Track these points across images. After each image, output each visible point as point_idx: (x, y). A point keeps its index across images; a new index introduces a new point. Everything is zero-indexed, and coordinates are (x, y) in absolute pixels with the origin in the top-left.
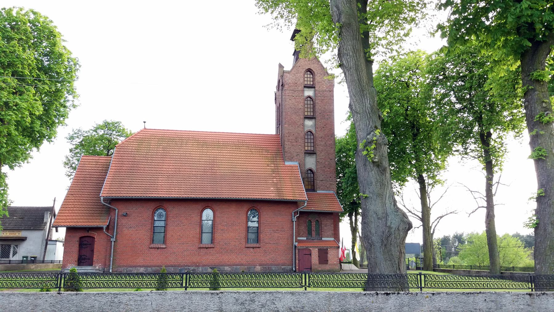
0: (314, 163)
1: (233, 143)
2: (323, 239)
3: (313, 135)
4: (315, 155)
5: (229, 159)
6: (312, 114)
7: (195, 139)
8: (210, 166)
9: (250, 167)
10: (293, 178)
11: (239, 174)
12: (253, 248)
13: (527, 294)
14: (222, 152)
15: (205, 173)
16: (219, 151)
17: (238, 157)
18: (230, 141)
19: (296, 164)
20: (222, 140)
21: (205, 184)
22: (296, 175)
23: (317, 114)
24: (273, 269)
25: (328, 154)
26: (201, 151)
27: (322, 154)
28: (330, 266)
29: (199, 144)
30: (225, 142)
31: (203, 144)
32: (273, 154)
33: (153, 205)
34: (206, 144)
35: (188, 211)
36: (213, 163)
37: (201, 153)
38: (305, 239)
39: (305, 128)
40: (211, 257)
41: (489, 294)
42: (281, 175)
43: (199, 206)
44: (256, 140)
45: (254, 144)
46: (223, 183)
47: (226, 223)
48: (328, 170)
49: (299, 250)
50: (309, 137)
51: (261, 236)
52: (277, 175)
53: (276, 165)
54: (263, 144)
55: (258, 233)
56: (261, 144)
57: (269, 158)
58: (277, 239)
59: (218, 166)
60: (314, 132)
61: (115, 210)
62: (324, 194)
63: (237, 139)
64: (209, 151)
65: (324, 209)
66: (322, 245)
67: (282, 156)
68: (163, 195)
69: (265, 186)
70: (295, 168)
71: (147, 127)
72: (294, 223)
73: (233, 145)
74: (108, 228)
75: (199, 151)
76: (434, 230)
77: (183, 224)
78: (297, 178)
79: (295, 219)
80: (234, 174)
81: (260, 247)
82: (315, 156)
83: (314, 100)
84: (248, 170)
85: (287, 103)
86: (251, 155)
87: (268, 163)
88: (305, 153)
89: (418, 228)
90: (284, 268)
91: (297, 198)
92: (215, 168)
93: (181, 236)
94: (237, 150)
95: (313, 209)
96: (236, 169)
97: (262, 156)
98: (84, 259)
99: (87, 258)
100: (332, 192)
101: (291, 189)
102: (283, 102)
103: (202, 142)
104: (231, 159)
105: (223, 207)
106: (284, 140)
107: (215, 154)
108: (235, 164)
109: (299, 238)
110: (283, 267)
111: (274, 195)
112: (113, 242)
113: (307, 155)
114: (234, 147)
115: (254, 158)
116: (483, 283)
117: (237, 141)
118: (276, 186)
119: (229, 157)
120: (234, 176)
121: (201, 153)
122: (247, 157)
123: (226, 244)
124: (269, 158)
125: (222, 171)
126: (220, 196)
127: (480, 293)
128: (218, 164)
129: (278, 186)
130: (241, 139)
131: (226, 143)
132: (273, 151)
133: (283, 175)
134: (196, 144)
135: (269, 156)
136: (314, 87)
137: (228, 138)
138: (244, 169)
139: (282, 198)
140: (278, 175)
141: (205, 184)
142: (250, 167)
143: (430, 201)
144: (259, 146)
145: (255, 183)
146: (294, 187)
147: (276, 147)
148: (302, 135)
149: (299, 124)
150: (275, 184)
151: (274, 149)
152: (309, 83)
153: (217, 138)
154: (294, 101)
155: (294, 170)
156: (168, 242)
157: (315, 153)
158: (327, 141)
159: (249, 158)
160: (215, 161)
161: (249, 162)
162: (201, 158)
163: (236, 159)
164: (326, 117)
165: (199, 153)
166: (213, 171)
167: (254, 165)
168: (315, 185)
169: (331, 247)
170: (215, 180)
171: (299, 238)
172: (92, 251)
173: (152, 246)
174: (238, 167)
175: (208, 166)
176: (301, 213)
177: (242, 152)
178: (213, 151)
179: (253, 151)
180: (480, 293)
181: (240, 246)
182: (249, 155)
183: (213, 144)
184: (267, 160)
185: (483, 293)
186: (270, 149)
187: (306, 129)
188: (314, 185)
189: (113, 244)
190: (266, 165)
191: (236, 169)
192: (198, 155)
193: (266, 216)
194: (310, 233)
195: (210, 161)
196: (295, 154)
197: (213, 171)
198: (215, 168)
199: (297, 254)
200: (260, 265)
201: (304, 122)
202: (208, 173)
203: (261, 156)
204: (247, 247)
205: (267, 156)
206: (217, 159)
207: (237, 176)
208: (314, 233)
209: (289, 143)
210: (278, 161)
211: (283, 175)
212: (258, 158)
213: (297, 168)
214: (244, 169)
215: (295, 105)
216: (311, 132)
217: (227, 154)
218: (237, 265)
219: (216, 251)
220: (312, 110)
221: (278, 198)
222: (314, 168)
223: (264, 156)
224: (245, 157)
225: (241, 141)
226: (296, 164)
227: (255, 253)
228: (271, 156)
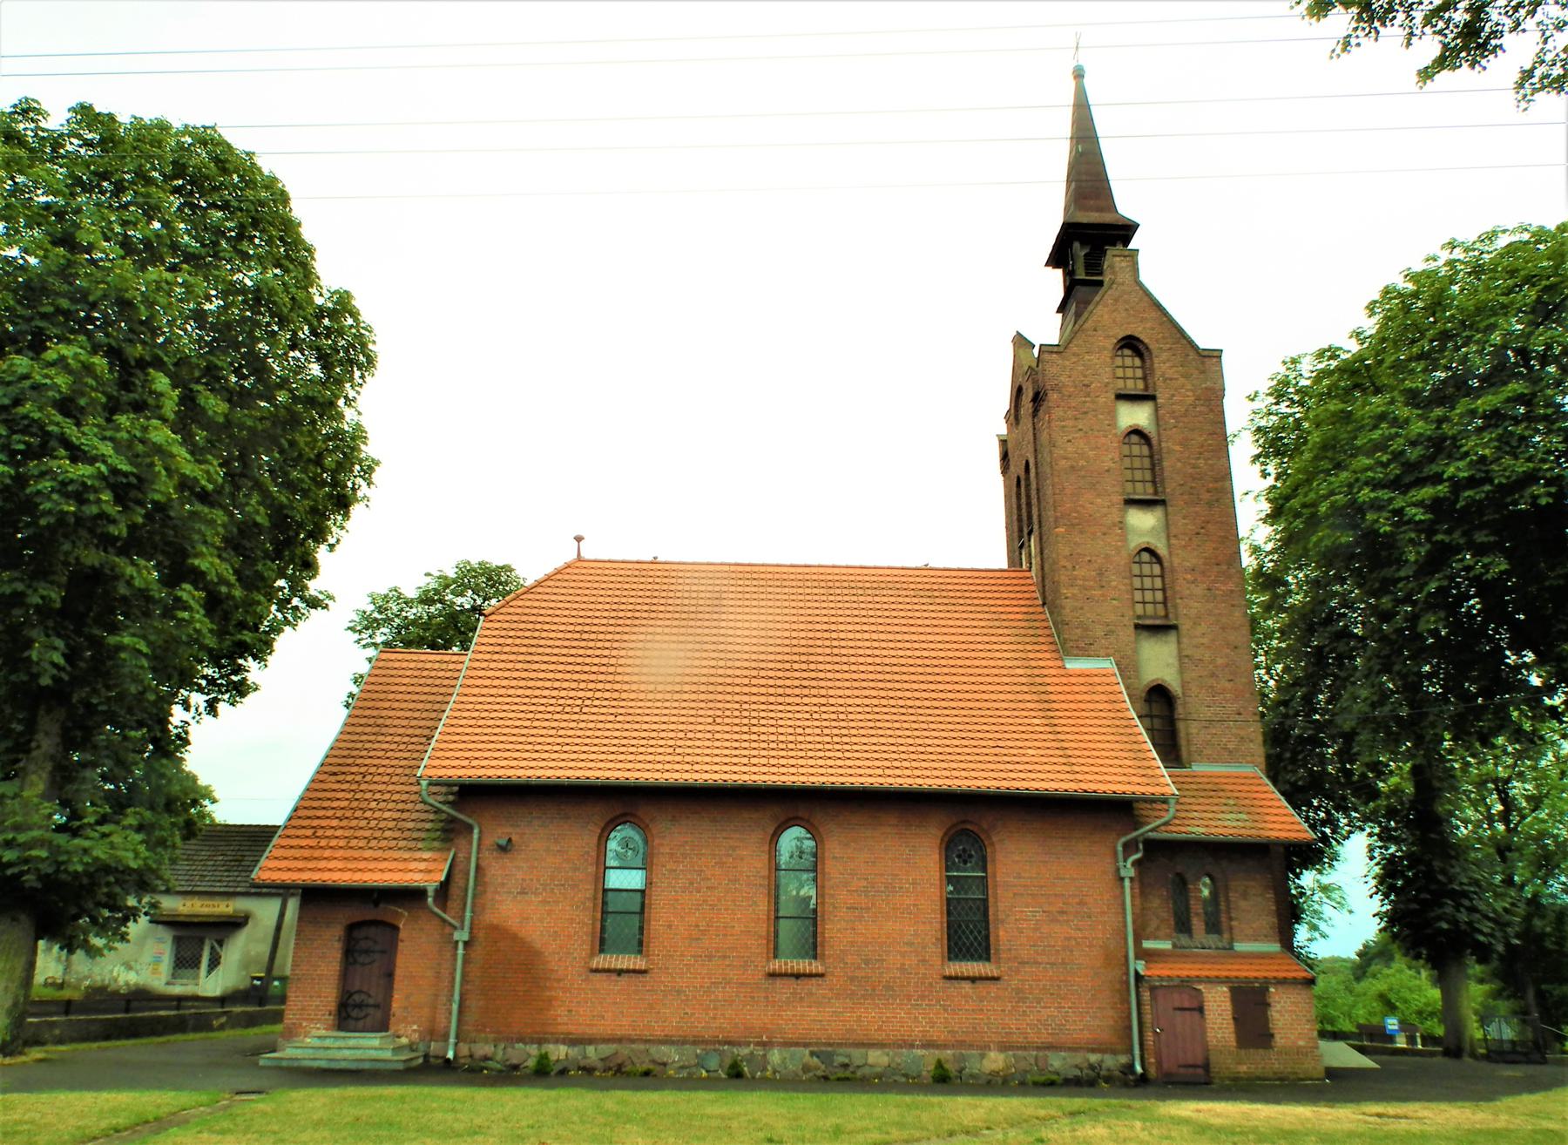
0: (1173, 661)
23: (1171, 487)
33: (598, 813)
35: (724, 834)
40: (813, 1013)
43: (768, 816)
48: (1228, 685)
49: (1153, 989)
51: (1001, 933)
60: (1162, 550)
61: (470, 828)
67: (1049, 639)
68: (608, 774)
71: (586, 555)
72: (1127, 883)
74: (444, 889)
77: (709, 884)
79: (1129, 871)
83: (1154, 442)
85: (1058, 452)
93: (703, 924)
98: (360, 1006)
99: (371, 1001)
102: (1045, 456)
106: (1056, 583)
109: (1147, 944)
112: (461, 945)
113: (1145, 634)
123: (867, 962)
147: (1024, 609)
152: (1130, 384)
156: (655, 947)
157: (1174, 627)
169: (1282, 982)
172: (390, 975)
173: (601, 961)
187: (1135, 542)
189: (460, 951)
194: (1183, 925)
199: (1147, 1008)
200: (1003, 1047)
201: (1123, 517)
208: (1198, 924)
209: (1075, 591)
222: (1171, 679)
226: (1108, 665)
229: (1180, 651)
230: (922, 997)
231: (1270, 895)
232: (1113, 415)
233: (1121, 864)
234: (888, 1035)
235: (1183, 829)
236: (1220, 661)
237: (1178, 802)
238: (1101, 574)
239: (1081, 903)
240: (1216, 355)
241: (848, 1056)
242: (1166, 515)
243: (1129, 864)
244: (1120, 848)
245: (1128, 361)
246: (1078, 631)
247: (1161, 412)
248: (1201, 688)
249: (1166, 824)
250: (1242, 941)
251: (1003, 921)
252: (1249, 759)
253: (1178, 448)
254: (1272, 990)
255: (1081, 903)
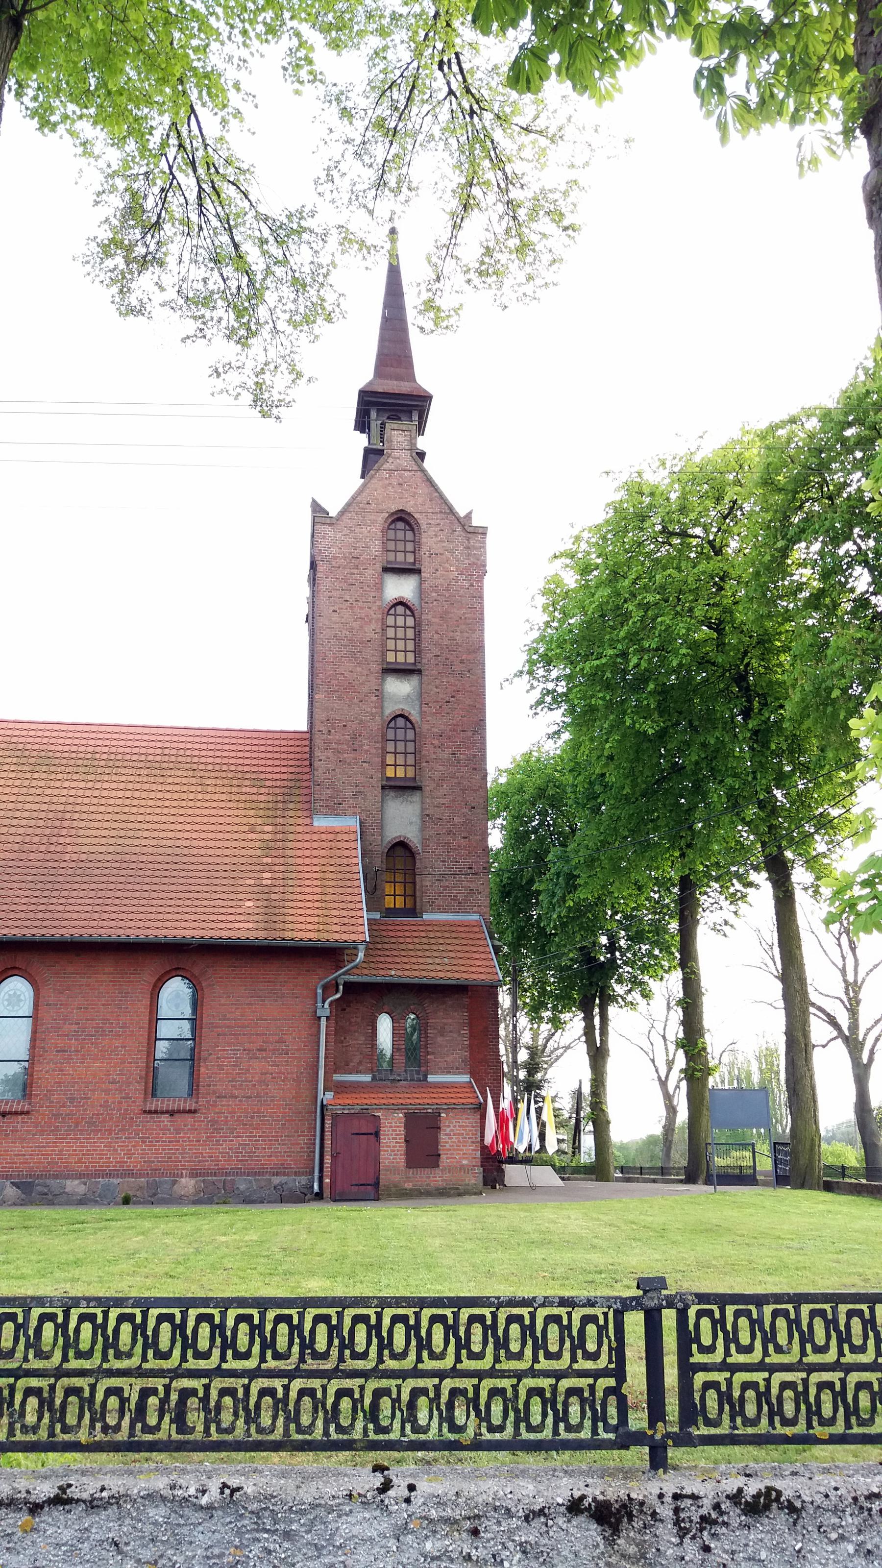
0: (416, 819)
1: (143, 758)
2: (431, 1078)
3: (414, 728)
4: (418, 793)
5: (117, 809)
6: (411, 658)
7: (12, 746)
8: (47, 831)
9: (186, 835)
10: (332, 869)
11: (144, 858)
12: (172, 1113)
13: (575, 1507)
14: (98, 785)
15: (23, 856)
16: (90, 785)
17: (151, 803)
18: (136, 750)
19: (353, 823)
20: (106, 749)
21: (10, 893)
22: (345, 861)
23: (427, 657)
24: (242, 1187)
25: (463, 790)
26: (26, 783)
27: (442, 792)
28: (447, 1176)
29: (23, 760)
30: (116, 754)
31: (40, 761)
32: (277, 791)
34: (48, 761)
36: (57, 823)
37: (24, 791)
38: (367, 1078)
39: (386, 704)
40: (17, 1148)
41: (158, 1513)
42: (291, 861)
44: (226, 747)
45: (218, 760)
46: (76, 886)
47: (75, 1027)
49: (335, 1117)
50: (400, 734)
51: (202, 1070)
52: (277, 861)
53: (279, 828)
54: (270, 769)
55: (192, 1060)
56: (240, 761)
57: (262, 805)
58: (260, 1082)
59: (73, 832)
60: (415, 716)
62: (451, 924)
63: (160, 745)
64: (52, 784)
65: (433, 974)
66: (421, 1100)
69: (225, 896)
70: (346, 837)
72: (323, 1022)
73: (142, 765)
75: (18, 782)
76: (872, 1052)
78: (348, 869)
79: (325, 1010)
80: (127, 858)
81: (195, 1112)
82: (416, 797)
84: (179, 843)
86: (200, 796)
87: (252, 821)
88: (383, 787)
89: (824, 1046)
90: (281, 1185)
91: (334, 935)
92: (62, 840)
94: (152, 779)
95: (394, 974)
96: (136, 842)
97: (237, 797)
100: (475, 917)
101: (317, 905)
103: (35, 754)
104: (126, 809)
105: (70, 969)
107: (72, 792)
108: (138, 826)
109: (337, 1077)
110: (276, 1180)
111: (250, 925)
113: (392, 794)
114: (142, 772)
115: (207, 804)
116: (139, 1384)
117: (159, 751)
118: (265, 896)
119: (119, 802)
120: (125, 865)
121: (24, 791)
122: (184, 804)
123: (72, 1099)
124: (262, 805)
125: (85, 849)
126: (53, 931)
127: (61, 1500)
128: (75, 824)
129: (274, 897)
130: (175, 745)
131: (119, 757)
132: (278, 783)
133: (299, 861)
134: (15, 760)
135: (262, 798)
136: (418, 572)
137: (130, 743)
138: (163, 842)
139: (276, 934)
140: (282, 861)
141: (10, 893)
142: (186, 835)
143: (856, 961)
144: (233, 768)
145: (192, 888)
146: (327, 898)
147: (292, 770)
148: (375, 725)
149: (365, 689)
150: (266, 889)
151: (285, 776)
152: (400, 557)
153: (92, 742)
154: (347, 615)
155: (340, 845)
157: (418, 788)
158: (459, 747)
159: (191, 804)
160: (68, 816)
161: (189, 819)
162: (19, 806)
163: (142, 810)
164: (458, 667)
165: (16, 790)
166: (52, 848)
167: (204, 828)
168: (418, 894)
169: (451, 1108)
170: (50, 879)
171: (337, 1077)
174: (146, 834)
175: (38, 831)
176: (350, 987)
177: (169, 788)
178: (66, 784)
179: (209, 782)
180: (61, 1500)
181: (124, 1106)
182: (192, 796)
183: (72, 762)
184: (252, 813)
185: (93, 1505)
186: (269, 776)
187: (390, 709)
188: (414, 896)
190: (246, 828)
191: (136, 842)
192: (13, 798)
193: (223, 1001)
195: (51, 815)
196: (349, 791)
197: (52, 848)
198: (62, 840)
199: (328, 1135)
200: (194, 1174)
201: (382, 684)
202: (32, 856)
203: (233, 797)
204: (150, 1112)
205: (254, 797)
206: (78, 808)
207: (133, 865)
209: (329, 753)
210: (291, 813)
211: (299, 861)
212: (222, 805)
213: (352, 837)
214: (163, 842)
215: (351, 630)
216: (407, 719)
217: (113, 794)
218: (110, 1175)
219: (36, 1125)
220: (411, 646)
221: (261, 934)
222: (412, 835)
223: (243, 797)
224: (175, 804)
225: (174, 752)
227: (178, 1131)
228: (270, 798)
229: (423, 809)
230: (123, 1130)
231: (465, 1031)
232: (380, 587)
233: (319, 1004)
234: (86, 1167)
235: (381, 972)
236: (457, 820)
237: (367, 949)
238: (354, 738)
239: (280, 1041)
240: (482, 532)
241: (46, 1186)
242: (421, 683)
243: (326, 1005)
244: (320, 991)
245: (400, 535)
246: (328, 791)
247: (425, 586)
248: (438, 844)
249: (356, 967)
250: (436, 1073)
251: (205, 1059)
252: (475, 909)
253: (437, 620)
254: (443, 1115)
255: (280, 1041)
